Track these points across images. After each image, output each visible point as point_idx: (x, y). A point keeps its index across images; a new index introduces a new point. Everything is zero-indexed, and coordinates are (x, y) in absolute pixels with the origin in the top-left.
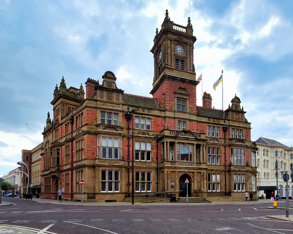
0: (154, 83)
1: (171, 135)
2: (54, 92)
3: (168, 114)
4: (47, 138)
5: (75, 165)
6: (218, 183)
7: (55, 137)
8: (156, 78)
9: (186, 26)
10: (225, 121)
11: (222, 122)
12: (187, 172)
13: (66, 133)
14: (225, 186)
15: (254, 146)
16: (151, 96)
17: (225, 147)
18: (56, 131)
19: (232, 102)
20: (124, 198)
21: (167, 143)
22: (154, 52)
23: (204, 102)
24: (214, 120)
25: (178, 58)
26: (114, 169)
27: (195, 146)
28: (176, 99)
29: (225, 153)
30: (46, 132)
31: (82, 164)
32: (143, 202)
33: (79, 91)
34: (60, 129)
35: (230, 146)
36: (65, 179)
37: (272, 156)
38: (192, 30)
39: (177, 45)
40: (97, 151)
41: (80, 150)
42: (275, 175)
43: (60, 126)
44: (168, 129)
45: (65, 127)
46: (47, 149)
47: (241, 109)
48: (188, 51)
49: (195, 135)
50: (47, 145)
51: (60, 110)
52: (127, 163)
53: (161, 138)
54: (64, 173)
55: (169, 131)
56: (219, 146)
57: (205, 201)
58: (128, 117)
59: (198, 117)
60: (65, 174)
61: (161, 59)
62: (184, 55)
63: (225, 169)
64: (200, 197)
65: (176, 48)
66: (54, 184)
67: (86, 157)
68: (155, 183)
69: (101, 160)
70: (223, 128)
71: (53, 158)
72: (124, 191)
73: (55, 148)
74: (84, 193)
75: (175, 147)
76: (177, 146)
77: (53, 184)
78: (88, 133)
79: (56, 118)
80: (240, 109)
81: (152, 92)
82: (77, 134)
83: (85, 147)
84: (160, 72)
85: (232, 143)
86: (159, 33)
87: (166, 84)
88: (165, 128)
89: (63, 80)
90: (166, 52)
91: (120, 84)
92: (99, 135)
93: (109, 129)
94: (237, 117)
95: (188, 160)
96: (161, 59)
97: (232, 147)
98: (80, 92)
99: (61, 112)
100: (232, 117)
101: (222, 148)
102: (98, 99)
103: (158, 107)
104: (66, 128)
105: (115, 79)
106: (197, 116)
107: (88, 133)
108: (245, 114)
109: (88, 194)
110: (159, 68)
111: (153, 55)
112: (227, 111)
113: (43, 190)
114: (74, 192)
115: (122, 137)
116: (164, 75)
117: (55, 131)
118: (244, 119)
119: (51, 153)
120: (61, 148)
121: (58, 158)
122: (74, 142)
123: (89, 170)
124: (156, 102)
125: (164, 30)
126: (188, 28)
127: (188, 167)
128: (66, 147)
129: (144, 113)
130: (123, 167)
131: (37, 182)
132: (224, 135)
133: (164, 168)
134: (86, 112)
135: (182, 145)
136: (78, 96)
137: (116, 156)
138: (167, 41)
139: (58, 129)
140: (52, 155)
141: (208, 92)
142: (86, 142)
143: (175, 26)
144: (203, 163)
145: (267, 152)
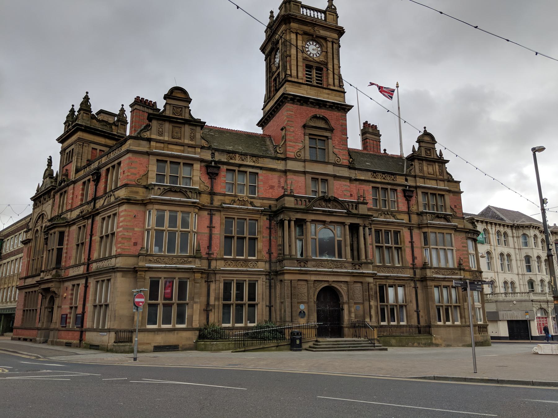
0: (265, 107)
1: (297, 207)
2: (65, 120)
3: (292, 165)
4: (41, 207)
5: (94, 266)
6: (401, 306)
7: (59, 208)
8: (269, 97)
9: (324, 8)
10: (408, 178)
11: (400, 180)
12: (334, 281)
13: (82, 200)
14: (418, 312)
15: (470, 226)
16: (259, 131)
17: (410, 229)
18: (61, 194)
19: (419, 141)
20: (197, 341)
21: (289, 221)
22: (266, 52)
23: (364, 141)
24: (384, 176)
25: (311, 64)
26: (178, 275)
27: (347, 227)
28: (307, 137)
29: (412, 242)
30: (40, 197)
31: (110, 265)
32: (238, 350)
33: (116, 118)
34: (72, 191)
35: (420, 227)
36: (70, 297)
37: (516, 244)
38: (337, 15)
39: (308, 41)
40: (143, 239)
41: (107, 236)
42: (527, 286)
43: (72, 186)
44: (292, 194)
45: (81, 187)
46: (37, 230)
47: (438, 154)
48: (329, 51)
49: (347, 206)
50: (40, 222)
51: (74, 154)
52: (205, 262)
53: (278, 210)
54: (69, 284)
55: (292, 199)
56: (398, 228)
57: (374, 346)
58: (212, 170)
59: (353, 171)
60: (71, 286)
61: (279, 64)
62: (322, 59)
63: (415, 273)
64: (362, 339)
65: (307, 46)
66: (45, 308)
67: (119, 250)
68: (264, 306)
69: (151, 258)
70: (404, 191)
71: (49, 251)
72: (196, 324)
73: (56, 230)
74: (109, 330)
75: (306, 228)
76: (311, 228)
77: (43, 307)
78: (128, 201)
79: (65, 168)
80: (435, 155)
81: (262, 124)
82: (105, 204)
83: (118, 230)
84: (276, 87)
85: (425, 222)
86: (274, 18)
87: (290, 110)
88: (286, 193)
89: (86, 99)
90: (288, 53)
91: (197, 111)
92: (150, 207)
93: (172, 193)
94: (431, 170)
95: (334, 256)
96: (279, 64)
97: (425, 230)
98: (118, 121)
99: (77, 158)
100: (421, 170)
101: (405, 232)
102: (153, 136)
103: (272, 152)
104: (83, 189)
105: (189, 101)
106: (350, 168)
107: (128, 201)
108: (447, 165)
109: (117, 332)
110: (275, 80)
111: (264, 56)
112: (411, 158)
113: (18, 322)
114: (88, 327)
115: (199, 210)
116: (283, 94)
117: (59, 194)
118: (445, 174)
119: (46, 239)
120: (69, 231)
121: (60, 251)
122: (98, 219)
123: (124, 279)
124: (268, 143)
125: (283, 16)
126: (327, 12)
127: (333, 272)
128: (80, 228)
129: (245, 163)
130: (198, 272)
131: (6, 299)
132: (406, 206)
133: (283, 274)
134: (127, 162)
135: (322, 226)
136: (113, 127)
137: (184, 248)
138: (290, 34)
139: (65, 192)
140: (47, 244)
141: (371, 122)
142: (121, 219)
143: (305, 10)
144: (365, 263)
145: (505, 237)
